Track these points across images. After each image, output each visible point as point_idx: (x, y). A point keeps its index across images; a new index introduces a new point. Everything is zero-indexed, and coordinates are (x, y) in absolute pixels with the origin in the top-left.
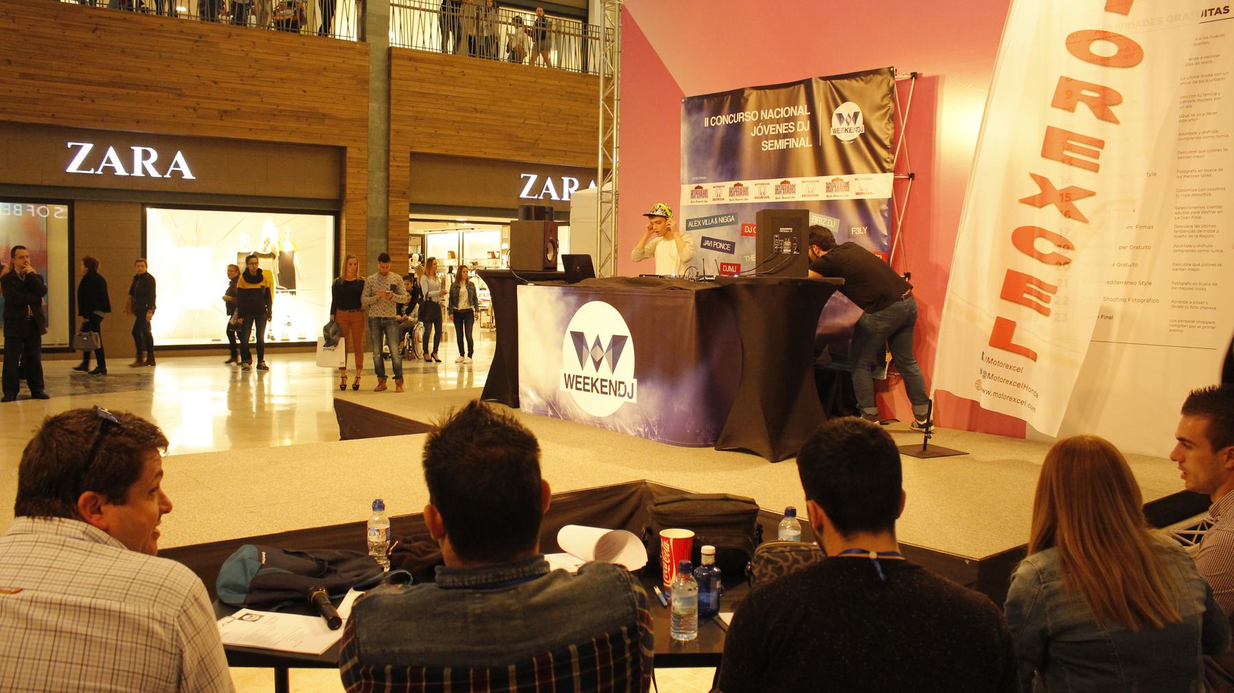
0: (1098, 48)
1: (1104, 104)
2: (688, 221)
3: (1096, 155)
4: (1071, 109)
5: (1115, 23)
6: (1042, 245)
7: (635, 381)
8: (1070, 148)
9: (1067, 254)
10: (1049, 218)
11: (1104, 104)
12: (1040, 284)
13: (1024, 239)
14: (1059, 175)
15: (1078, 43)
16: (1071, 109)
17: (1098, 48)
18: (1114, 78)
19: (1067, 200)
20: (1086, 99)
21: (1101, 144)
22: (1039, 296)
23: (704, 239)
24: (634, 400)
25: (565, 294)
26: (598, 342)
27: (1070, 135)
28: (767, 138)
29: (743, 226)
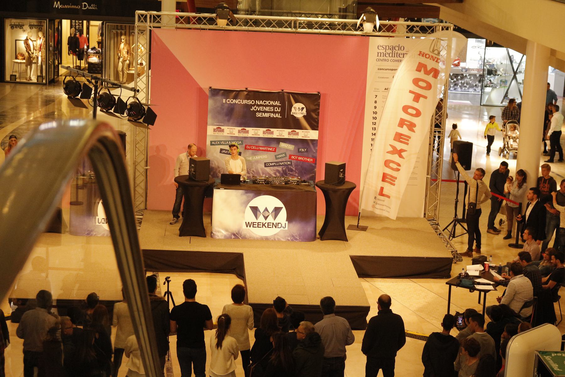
0: (410, 111)
1: (411, 127)
2: (211, 142)
3: (408, 140)
4: (402, 127)
5: (416, 105)
6: (392, 165)
7: (287, 222)
8: (402, 138)
9: (399, 167)
10: (396, 158)
11: (411, 127)
12: (391, 176)
13: (387, 163)
14: (399, 146)
15: (405, 109)
16: (402, 127)
17: (410, 111)
18: (415, 120)
19: (400, 153)
20: (406, 125)
21: (410, 137)
22: (391, 179)
23: (221, 150)
24: (286, 228)
25: (246, 193)
26: (266, 210)
27: (402, 135)
28: (260, 111)
29: (246, 146)
